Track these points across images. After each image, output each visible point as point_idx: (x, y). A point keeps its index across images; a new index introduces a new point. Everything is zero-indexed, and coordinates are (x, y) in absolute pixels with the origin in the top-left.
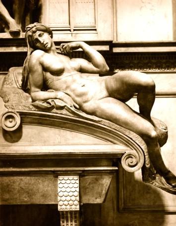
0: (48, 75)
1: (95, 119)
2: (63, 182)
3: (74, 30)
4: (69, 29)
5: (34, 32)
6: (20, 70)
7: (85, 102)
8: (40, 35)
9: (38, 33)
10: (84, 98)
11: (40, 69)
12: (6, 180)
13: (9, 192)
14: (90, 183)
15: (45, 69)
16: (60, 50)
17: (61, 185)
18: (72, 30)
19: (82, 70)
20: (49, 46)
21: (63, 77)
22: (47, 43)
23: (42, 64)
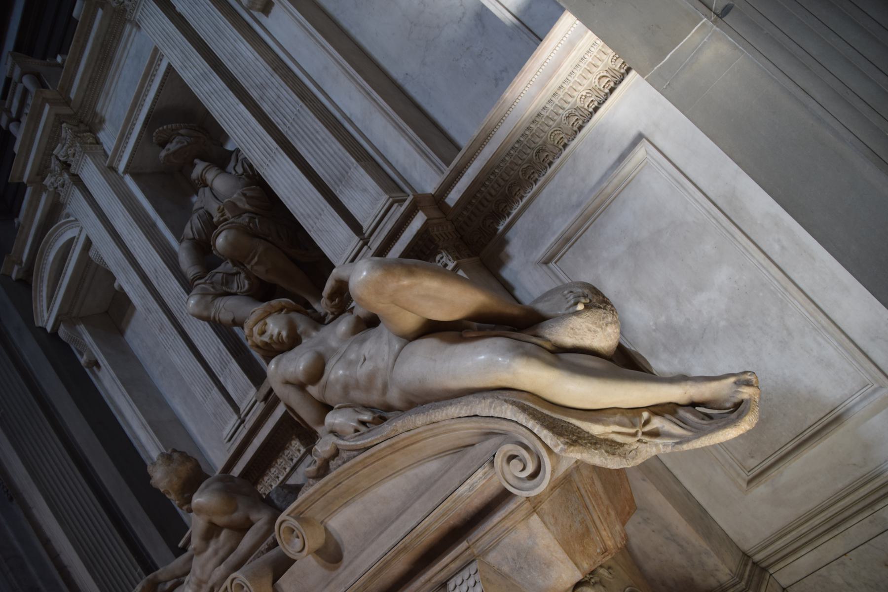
5: (251, 335)
8: (263, 333)
10: (379, 383)
13: (548, 567)
15: (301, 387)
21: (336, 372)
22: (279, 334)
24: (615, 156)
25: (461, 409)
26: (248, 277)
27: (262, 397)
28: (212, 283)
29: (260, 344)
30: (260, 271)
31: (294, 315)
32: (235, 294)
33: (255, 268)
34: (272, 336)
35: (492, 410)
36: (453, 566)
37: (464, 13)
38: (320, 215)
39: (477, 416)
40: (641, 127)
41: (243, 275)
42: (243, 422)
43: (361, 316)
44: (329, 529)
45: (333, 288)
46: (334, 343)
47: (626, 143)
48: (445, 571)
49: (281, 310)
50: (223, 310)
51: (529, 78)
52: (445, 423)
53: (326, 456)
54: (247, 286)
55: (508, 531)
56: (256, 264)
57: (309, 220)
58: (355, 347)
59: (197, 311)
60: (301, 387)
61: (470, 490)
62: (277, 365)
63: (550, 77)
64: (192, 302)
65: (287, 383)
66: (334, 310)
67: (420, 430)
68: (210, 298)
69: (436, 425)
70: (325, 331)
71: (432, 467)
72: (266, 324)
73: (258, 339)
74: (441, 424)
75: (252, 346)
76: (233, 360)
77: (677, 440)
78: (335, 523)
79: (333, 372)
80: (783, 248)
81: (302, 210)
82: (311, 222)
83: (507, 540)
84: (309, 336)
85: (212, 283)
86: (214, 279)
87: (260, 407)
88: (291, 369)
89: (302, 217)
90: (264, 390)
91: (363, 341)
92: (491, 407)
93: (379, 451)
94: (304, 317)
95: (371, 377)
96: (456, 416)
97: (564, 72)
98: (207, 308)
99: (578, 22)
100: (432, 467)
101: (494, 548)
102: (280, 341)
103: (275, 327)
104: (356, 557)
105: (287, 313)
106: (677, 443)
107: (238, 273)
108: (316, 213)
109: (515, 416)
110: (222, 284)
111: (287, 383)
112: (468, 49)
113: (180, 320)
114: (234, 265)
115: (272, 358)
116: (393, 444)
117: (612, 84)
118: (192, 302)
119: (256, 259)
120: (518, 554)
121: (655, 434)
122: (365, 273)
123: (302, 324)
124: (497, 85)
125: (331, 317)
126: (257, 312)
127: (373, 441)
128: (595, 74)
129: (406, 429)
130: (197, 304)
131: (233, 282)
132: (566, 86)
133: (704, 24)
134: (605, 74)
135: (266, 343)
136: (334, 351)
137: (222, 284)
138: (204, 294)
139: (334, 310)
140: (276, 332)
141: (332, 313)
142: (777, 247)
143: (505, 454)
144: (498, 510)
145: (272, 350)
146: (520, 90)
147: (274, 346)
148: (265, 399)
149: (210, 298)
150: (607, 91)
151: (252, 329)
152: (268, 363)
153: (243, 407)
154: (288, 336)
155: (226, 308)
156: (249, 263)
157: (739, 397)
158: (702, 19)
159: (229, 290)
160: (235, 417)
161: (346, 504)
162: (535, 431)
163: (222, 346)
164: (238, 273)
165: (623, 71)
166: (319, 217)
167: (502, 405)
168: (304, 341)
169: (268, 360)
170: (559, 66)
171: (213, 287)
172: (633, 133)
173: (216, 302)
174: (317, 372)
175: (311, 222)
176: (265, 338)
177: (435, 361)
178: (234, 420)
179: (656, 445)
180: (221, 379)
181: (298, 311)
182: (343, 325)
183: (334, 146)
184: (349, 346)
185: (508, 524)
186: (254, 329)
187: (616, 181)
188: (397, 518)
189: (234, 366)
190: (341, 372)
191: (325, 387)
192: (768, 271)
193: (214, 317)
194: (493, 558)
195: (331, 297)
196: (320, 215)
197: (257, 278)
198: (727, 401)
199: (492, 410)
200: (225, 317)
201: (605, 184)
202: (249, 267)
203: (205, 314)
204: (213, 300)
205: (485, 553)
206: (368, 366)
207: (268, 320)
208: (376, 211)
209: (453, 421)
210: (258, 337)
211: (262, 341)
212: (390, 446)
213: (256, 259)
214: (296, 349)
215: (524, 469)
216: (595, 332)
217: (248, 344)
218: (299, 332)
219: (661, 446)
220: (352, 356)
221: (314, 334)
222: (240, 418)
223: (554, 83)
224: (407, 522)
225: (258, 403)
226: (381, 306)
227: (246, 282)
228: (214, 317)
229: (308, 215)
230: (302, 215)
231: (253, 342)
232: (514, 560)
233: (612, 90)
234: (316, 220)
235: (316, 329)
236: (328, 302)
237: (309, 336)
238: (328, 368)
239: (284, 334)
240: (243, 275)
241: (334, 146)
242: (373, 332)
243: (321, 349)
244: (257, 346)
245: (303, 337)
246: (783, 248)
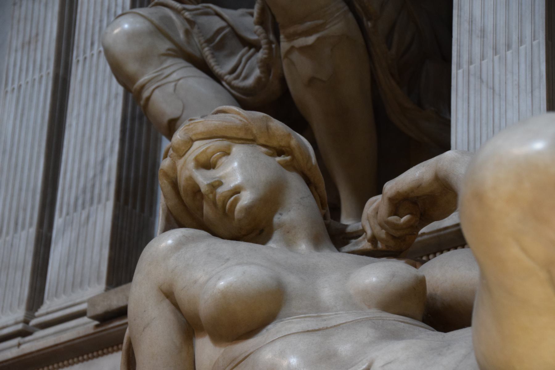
5: (180, 153)
8: (207, 165)
9: (198, 147)
15: (190, 327)
22: (237, 191)
26: (267, 66)
27: (100, 309)
28: (191, 23)
29: (182, 182)
30: (299, 71)
31: (295, 181)
32: (217, 78)
33: (296, 57)
34: (220, 183)
38: (508, 47)
41: (261, 55)
42: (24, 333)
45: (419, 186)
46: (327, 291)
49: (279, 152)
50: (170, 88)
54: (250, 81)
56: (303, 50)
58: (365, 334)
59: (119, 48)
60: (190, 327)
62: (179, 245)
64: (126, 25)
65: (169, 295)
66: (382, 234)
68: (164, 46)
70: (330, 258)
72: (227, 153)
73: (187, 169)
76: (110, 205)
79: (278, 346)
81: (477, 13)
82: (477, 50)
84: (289, 243)
85: (191, 23)
86: (203, 20)
87: (84, 327)
88: (200, 275)
89: (466, 26)
90: (115, 300)
91: (395, 336)
94: (310, 201)
98: (144, 59)
102: (225, 210)
103: (239, 173)
105: (287, 166)
107: (255, 46)
108: (502, 40)
110: (209, 41)
111: (169, 295)
113: (77, 54)
114: (261, 22)
115: (181, 226)
118: (126, 25)
119: (311, 40)
122: (539, 145)
123: (297, 208)
125: (365, 244)
126: (228, 116)
130: (132, 36)
131: (232, 54)
135: (196, 191)
136: (316, 308)
137: (209, 41)
138: (160, 30)
139: (382, 234)
141: (374, 240)
145: (199, 212)
147: (207, 209)
148: (105, 318)
149: (164, 46)
151: (192, 141)
152: (168, 227)
153: (52, 305)
154: (249, 209)
155: (177, 88)
156: (290, 37)
159: (211, 62)
160: (20, 313)
163: (112, 162)
164: (255, 46)
166: (502, 48)
168: (271, 244)
169: (172, 223)
171: (187, 33)
173: (170, 61)
175: (477, 50)
176: (203, 179)
178: (11, 317)
180: (58, 222)
181: (309, 182)
182: (378, 275)
186: (197, 144)
189: (103, 216)
190: (293, 361)
193: (143, 87)
195: (398, 204)
197: (283, 80)
200: (164, 103)
202: (285, 45)
203: (132, 67)
204: (168, 54)
207: (238, 150)
210: (191, 165)
211: (191, 179)
213: (311, 40)
214: (243, 246)
217: (165, 164)
218: (277, 219)
220: (344, 348)
221: (303, 247)
222: (26, 322)
225: (85, 319)
226: (514, 251)
227: (257, 72)
228: (143, 87)
229: (483, 31)
230: (471, 21)
231: (174, 167)
234: (490, 52)
235: (316, 243)
236: (384, 210)
237: (289, 243)
238: (273, 330)
239: (246, 198)
240: (261, 55)
242: (430, 337)
243: (292, 281)
244: (175, 184)
245: (276, 235)
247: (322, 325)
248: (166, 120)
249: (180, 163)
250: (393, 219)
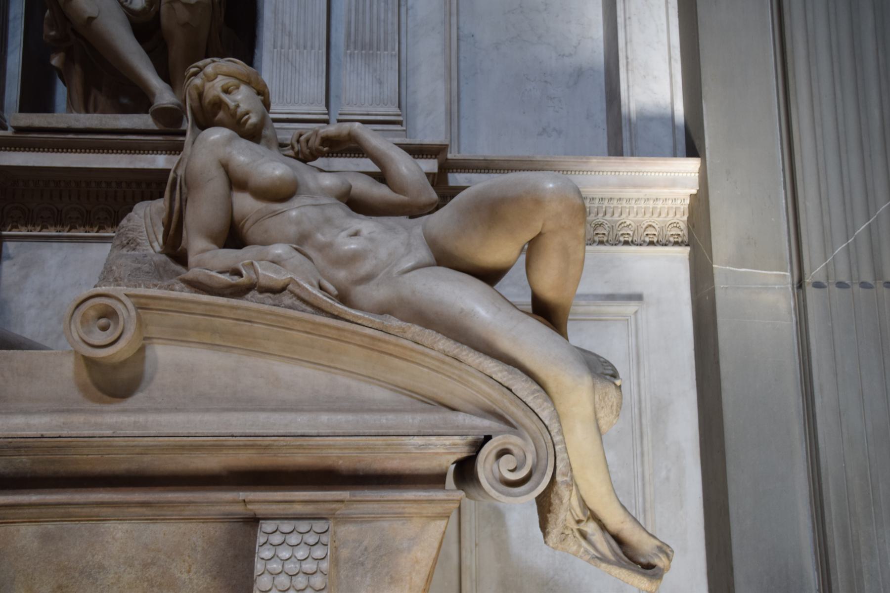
0: (244, 203)
1: (440, 88)
2: (277, 539)
3: (339, 121)
4: (326, 117)
5: (210, 79)
6: (160, 204)
7: (367, 279)
10: (365, 268)
11: (216, 184)
12: (3, 512)
13: (390, 583)
14: (445, 445)
15: (236, 182)
16: (293, 148)
17: (266, 553)
18: (333, 120)
19: (358, 205)
20: (253, 119)
21: (294, 210)
22: (247, 113)
23: (225, 167)
24: (607, 290)
25: (501, 371)
35: (531, 397)
36: (299, 509)
37: (570, 55)
38: (305, 48)
39: (510, 390)
40: (646, 293)
43: (353, 191)
44: (148, 352)
47: (625, 291)
48: (282, 506)
51: (620, 169)
52: (469, 369)
53: (263, 282)
55: (400, 516)
57: (286, 39)
61: (420, 447)
63: (635, 186)
67: (433, 353)
69: (456, 363)
71: (381, 394)
72: (238, 88)
74: (463, 366)
75: (197, 88)
77: (599, 556)
78: (164, 355)
80: (667, 479)
81: (287, 22)
83: (385, 524)
92: (533, 394)
93: (354, 333)
95: (354, 258)
96: (488, 372)
97: (631, 193)
99: (697, 175)
100: (381, 394)
101: (362, 522)
104: (158, 411)
106: (597, 557)
109: (551, 419)
112: (546, 82)
116: (379, 340)
117: (655, 240)
120: (379, 547)
121: (584, 535)
124: (540, 134)
127: (360, 318)
128: (651, 219)
129: (418, 339)
132: (615, 203)
133: (785, 275)
134: (657, 227)
140: (243, 107)
142: (663, 474)
143: (505, 443)
144: (418, 489)
146: (603, 169)
150: (647, 239)
157: (655, 561)
158: (786, 271)
161: (213, 346)
162: (557, 448)
165: (672, 239)
167: (545, 401)
170: (650, 187)
172: (636, 289)
174: (280, 194)
177: (500, 310)
179: (580, 546)
183: (390, 15)
184: (331, 204)
185: (410, 509)
187: (593, 309)
188: (274, 410)
191: (275, 214)
192: (644, 485)
194: (347, 531)
196: (305, 48)
198: (643, 556)
199: (531, 397)
201: (583, 303)
205: (346, 520)
206: (353, 245)
207: (243, 88)
208: (372, 110)
209: (480, 375)
210: (219, 89)
212: (373, 338)
215: (512, 471)
216: (612, 413)
219: (582, 550)
223: (631, 193)
224: (300, 422)
231: (203, 86)
232: (366, 549)
233: (651, 243)
241: (390, 15)
246: (667, 479)
247: (318, 203)
248: (87, 16)
249: (208, 85)
250: (321, 148)
